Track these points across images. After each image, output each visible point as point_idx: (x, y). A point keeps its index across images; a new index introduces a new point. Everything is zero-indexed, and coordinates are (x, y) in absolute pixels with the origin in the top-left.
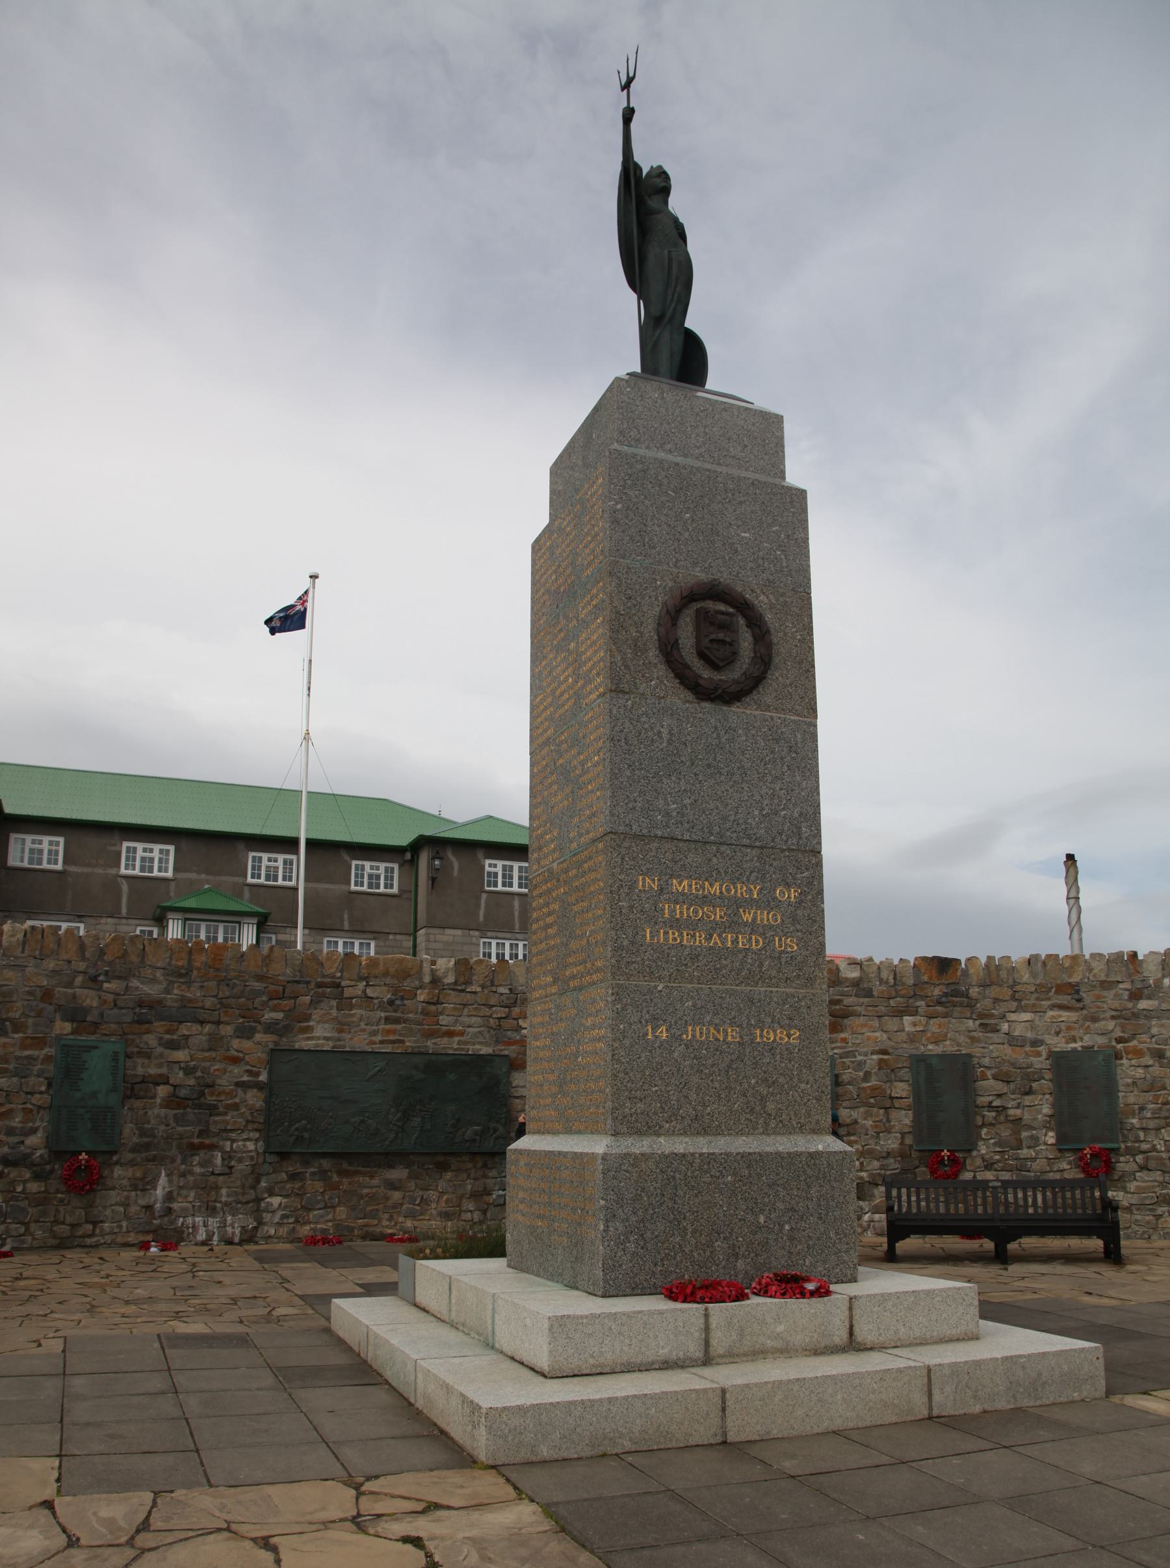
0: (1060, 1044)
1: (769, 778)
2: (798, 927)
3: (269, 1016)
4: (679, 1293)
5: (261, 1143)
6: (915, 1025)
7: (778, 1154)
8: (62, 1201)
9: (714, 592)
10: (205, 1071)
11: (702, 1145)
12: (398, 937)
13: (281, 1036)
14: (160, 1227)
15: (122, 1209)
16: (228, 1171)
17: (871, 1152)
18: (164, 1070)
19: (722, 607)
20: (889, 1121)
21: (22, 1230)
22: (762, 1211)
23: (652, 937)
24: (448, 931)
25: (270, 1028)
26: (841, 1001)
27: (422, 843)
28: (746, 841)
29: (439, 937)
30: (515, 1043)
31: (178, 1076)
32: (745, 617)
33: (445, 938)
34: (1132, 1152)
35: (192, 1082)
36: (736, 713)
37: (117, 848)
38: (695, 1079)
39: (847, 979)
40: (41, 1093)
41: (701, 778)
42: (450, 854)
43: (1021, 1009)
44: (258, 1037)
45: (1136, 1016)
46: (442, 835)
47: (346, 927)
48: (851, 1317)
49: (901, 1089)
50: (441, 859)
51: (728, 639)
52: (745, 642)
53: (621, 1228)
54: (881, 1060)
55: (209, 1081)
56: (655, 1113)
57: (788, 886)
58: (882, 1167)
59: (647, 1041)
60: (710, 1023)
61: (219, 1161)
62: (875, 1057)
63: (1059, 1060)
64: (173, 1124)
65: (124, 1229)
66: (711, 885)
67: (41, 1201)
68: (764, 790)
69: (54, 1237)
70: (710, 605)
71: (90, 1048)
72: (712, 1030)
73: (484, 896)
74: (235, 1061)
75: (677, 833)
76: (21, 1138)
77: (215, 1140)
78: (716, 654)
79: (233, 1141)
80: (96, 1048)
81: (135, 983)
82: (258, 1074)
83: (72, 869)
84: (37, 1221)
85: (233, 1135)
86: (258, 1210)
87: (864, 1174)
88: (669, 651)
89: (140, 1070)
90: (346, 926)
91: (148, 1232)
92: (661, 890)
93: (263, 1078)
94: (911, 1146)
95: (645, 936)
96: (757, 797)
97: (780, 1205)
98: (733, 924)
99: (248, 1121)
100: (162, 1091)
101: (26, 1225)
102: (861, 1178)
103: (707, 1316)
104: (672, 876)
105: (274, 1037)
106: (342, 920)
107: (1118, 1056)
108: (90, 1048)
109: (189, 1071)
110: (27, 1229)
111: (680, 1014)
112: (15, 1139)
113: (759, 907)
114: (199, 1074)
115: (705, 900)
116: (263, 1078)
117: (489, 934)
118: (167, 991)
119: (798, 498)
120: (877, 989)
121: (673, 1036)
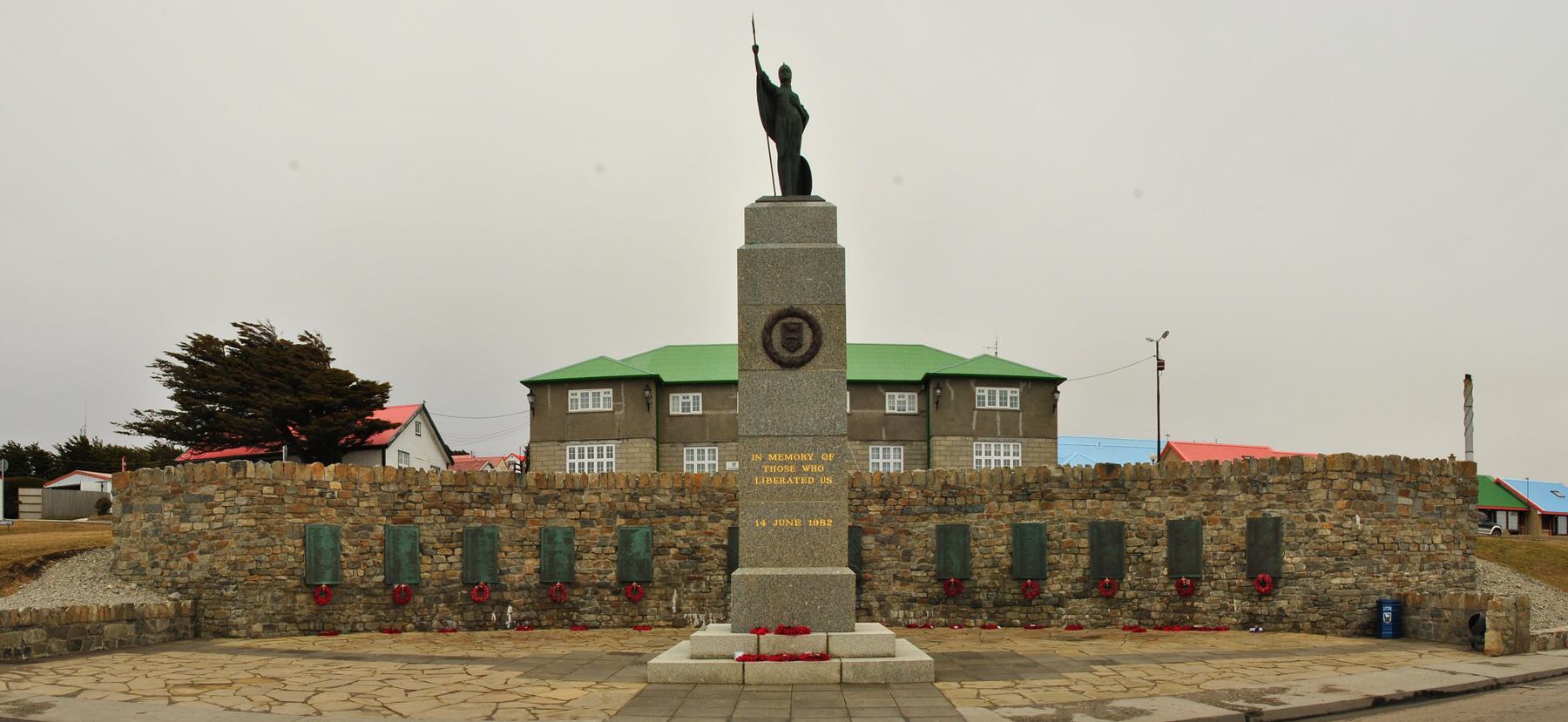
0: (1173, 516)
3: (727, 510)
4: (752, 632)
9: (791, 313)
11: (780, 571)
19: (796, 320)
27: (929, 378)
31: (681, 544)
34: (1209, 579)
36: (801, 373)
43: (1153, 495)
45: (1215, 499)
49: (1084, 542)
63: (1172, 525)
67: (616, 605)
70: (806, 325)
74: (710, 534)
78: (792, 343)
88: (767, 345)
98: (799, 472)
107: (1203, 523)
109: (685, 541)
115: (785, 463)
119: (840, 254)
120: (1073, 483)
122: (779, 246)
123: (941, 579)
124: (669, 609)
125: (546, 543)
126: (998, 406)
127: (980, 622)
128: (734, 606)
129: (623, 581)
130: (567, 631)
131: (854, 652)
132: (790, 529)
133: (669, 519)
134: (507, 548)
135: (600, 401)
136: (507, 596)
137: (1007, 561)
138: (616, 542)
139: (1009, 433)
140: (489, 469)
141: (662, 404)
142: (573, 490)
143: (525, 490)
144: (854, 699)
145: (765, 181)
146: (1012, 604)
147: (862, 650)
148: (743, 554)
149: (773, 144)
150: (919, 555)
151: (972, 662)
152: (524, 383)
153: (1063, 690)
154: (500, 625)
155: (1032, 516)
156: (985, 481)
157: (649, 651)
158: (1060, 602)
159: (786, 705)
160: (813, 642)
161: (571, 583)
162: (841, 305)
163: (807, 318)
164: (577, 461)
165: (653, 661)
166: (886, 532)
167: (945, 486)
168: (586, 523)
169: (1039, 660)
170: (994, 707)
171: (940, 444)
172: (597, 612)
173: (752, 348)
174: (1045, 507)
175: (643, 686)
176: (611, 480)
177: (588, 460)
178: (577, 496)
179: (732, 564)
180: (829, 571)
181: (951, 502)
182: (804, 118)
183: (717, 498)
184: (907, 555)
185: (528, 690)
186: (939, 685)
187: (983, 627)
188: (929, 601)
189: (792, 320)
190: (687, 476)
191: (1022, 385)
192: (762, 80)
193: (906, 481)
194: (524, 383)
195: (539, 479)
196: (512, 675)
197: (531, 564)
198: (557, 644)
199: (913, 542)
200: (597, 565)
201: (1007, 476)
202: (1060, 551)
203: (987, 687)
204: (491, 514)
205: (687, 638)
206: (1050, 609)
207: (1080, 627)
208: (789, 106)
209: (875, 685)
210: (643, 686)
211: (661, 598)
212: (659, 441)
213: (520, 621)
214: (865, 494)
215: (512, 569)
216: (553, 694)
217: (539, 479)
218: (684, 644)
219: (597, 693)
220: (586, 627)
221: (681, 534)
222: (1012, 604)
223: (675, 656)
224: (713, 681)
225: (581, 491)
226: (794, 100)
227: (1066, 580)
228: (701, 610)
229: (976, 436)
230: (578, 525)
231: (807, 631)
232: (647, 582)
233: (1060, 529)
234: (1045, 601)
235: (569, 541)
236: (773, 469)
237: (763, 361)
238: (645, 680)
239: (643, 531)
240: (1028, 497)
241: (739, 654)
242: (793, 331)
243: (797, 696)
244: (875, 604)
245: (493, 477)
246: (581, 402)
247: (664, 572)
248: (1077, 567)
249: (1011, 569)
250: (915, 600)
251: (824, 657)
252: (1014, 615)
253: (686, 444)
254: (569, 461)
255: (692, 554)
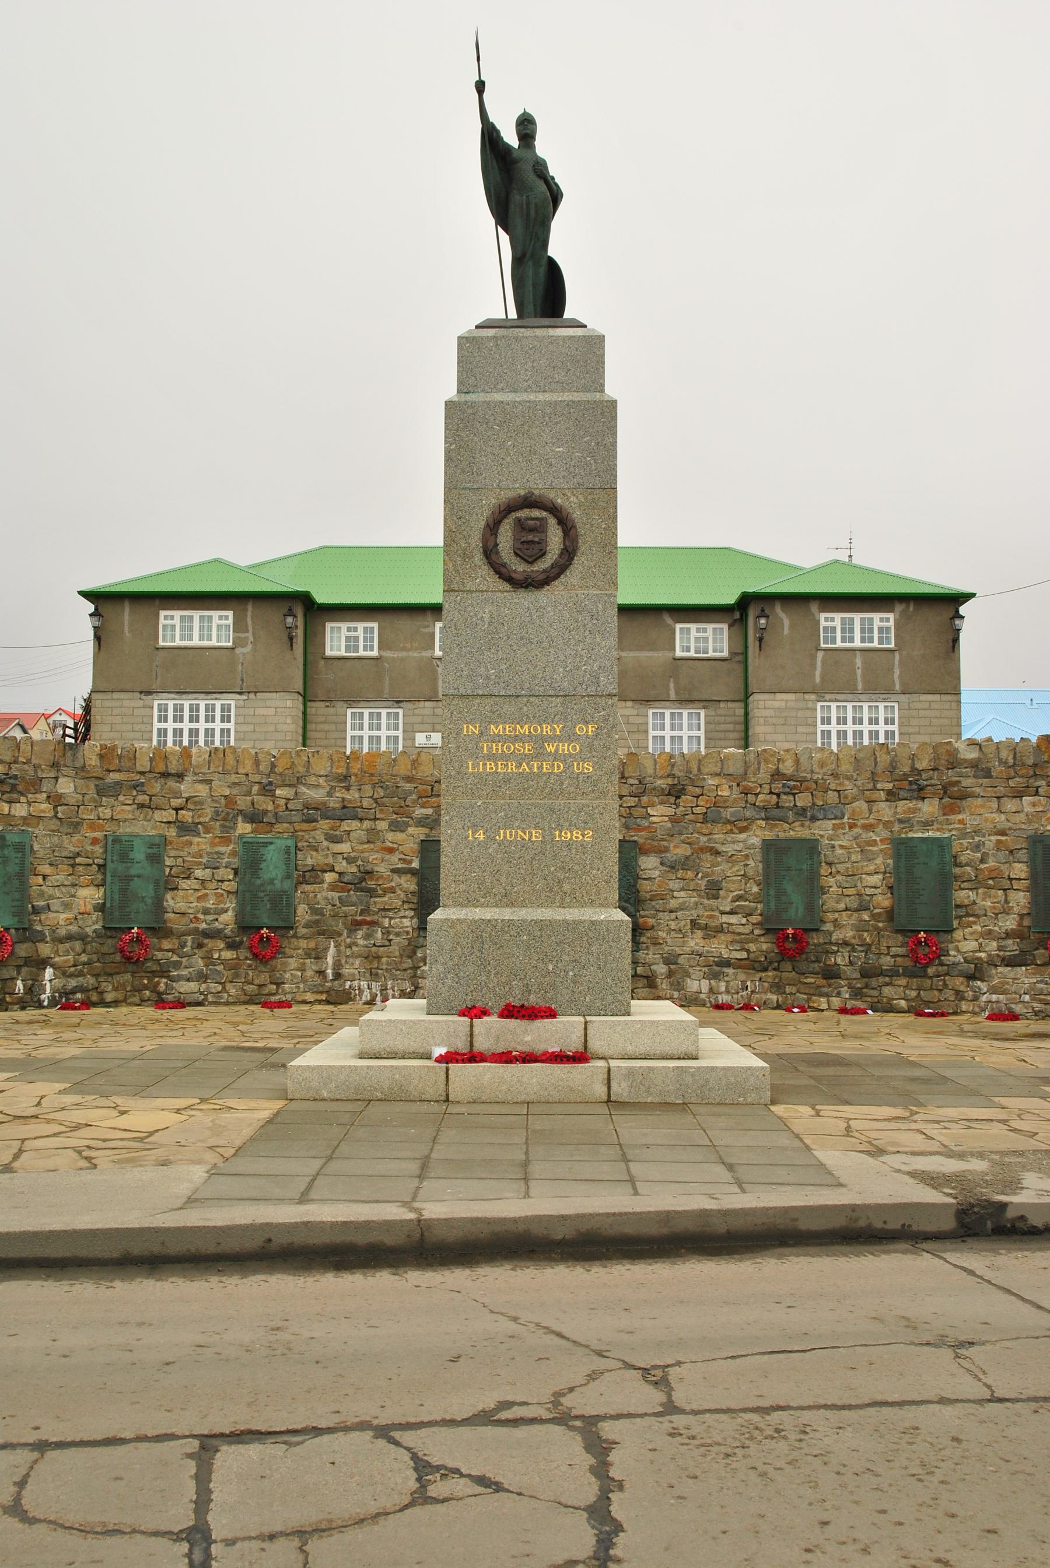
1: (573, 642)
2: (594, 753)
3: (419, 812)
4: (462, 1014)
5: (415, 920)
6: (1034, 805)
7: (565, 921)
8: (250, 966)
9: (529, 502)
10: (366, 861)
11: (507, 914)
12: (730, 705)
13: (431, 829)
14: (331, 989)
15: (299, 974)
16: (387, 943)
17: (990, 932)
18: (330, 860)
19: (536, 513)
20: (1007, 902)
21: (220, 988)
22: (551, 961)
23: (473, 768)
24: (779, 696)
25: (421, 822)
26: (960, 782)
27: (746, 601)
28: (551, 692)
29: (769, 703)
30: (644, 829)
31: (342, 865)
32: (555, 516)
33: (777, 704)
35: (354, 869)
36: (543, 596)
37: (430, 630)
38: (505, 867)
39: (965, 760)
40: (230, 880)
41: (515, 648)
42: (778, 609)
44: (411, 830)
46: (768, 590)
47: (673, 696)
48: (586, 1035)
49: (1020, 870)
50: (767, 617)
51: (536, 539)
52: (555, 539)
53: (441, 969)
54: (999, 842)
55: (369, 868)
56: (474, 892)
57: (587, 723)
58: (1000, 948)
59: (469, 841)
60: (519, 828)
61: (379, 935)
62: (992, 838)
64: (339, 905)
65: (302, 990)
66: (522, 727)
67: (233, 967)
68: (569, 651)
69: (246, 995)
70: (552, 521)
71: (266, 844)
72: (520, 832)
73: (820, 654)
74: (391, 851)
75: (496, 692)
76: (216, 917)
77: (375, 918)
78: (530, 546)
79: (391, 918)
80: (272, 843)
81: (303, 789)
82: (410, 862)
83: (387, 654)
84: (231, 982)
85: (391, 914)
86: (415, 976)
87: (983, 955)
88: (490, 553)
89: (309, 861)
90: (673, 696)
91: (322, 993)
92: (482, 733)
93: (415, 864)
94: (1029, 927)
95: (468, 767)
96: (562, 658)
97: (566, 958)
98: (539, 754)
99: (404, 902)
100: (329, 877)
101: (223, 984)
102: (980, 959)
103: (472, 1026)
104: (490, 723)
105: (427, 831)
106: (668, 688)
108: (266, 844)
109: (350, 861)
110: (224, 988)
111: (494, 822)
112: (210, 918)
113: (562, 741)
114: (359, 862)
115: (516, 739)
116: (415, 864)
117: (828, 697)
118: (330, 794)
119: (612, 405)
120: (997, 769)
121: (489, 837)
122: (510, 397)
123: (772, 929)
124: (321, 973)
125: (114, 862)
126: (857, 643)
127: (836, 1002)
128: (432, 972)
129: (246, 927)
130: (149, 1011)
131: (630, 1049)
132: (524, 845)
133: (324, 824)
134: (46, 869)
135: (214, 629)
136: (45, 950)
137: (884, 901)
138: (236, 862)
139: (877, 687)
140: (18, 734)
141: (313, 638)
142: (166, 775)
143: (82, 772)
144: (632, 1129)
145: (493, 297)
146: (893, 973)
147: (644, 1045)
148: (447, 886)
149: (505, 238)
150: (733, 888)
151: (831, 1071)
152: (87, 595)
153: (997, 1129)
154: (31, 1000)
155: (927, 824)
156: (845, 767)
157: (287, 1044)
158: (976, 972)
159: (519, 1138)
160: (560, 1032)
161: (160, 930)
162: (611, 490)
163: (555, 510)
164: (170, 726)
165: (297, 1062)
166: (679, 851)
167: (777, 775)
168: (185, 829)
169: (948, 1073)
170: (878, 1152)
171: (763, 705)
172: (202, 977)
173: (466, 556)
174: (949, 810)
175: (279, 1104)
176: (230, 759)
177: (182, 723)
178: (172, 783)
179: (426, 901)
180: (588, 914)
181: (787, 801)
182: (555, 197)
183: (406, 792)
184: (714, 889)
185: (78, 1116)
186: (778, 1109)
187: (843, 1011)
188: (751, 965)
189: (530, 532)
190: (355, 755)
191: (899, 607)
192: (490, 136)
193: (710, 767)
194: (87, 595)
195: (106, 754)
196: (48, 1088)
197: (89, 896)
198: (132, 1032)
199: (722, 868)
200: (201, 900)
201: (883, 759)
202: (976, 883)
203: (864, 1116)
204: (20, 810)
205: (355, 1023)
206: (959, 983)
207: (1015, 1017)
208: (531, 177)
209: (666, 1106)
210: (279, 1104)
211: (308, 955)
212: (306, 697)
213: (67, 993)
214: (642, 789)
215: (55, 904)
216: (123, 1122)
217: (106, 754)
218: (348, 1033)
219: (202, 1118)
220: (180, 1004)
221: (344, 849)
222: (893, 973)
223: (332, 1052)
224: (396, 1096)
225: (180, 776)
226: (540, 169)
227: (989, 934)
228: (374, 976)
229: (820, 693)
230: (172, 832)
231: (552, 1014)
232: (287, 928)
233: (977, 847)
234: (951, 970)
235: (156, 859)
236: (497, 748)
237: (483, 576)
238: (283, 1094)
239: (281, 843)
240: (920, 793)
241: (439, 1051)
242: (532, 530)
243: (536, 1124)
244: (661, 969)
245: (25, 748)
246: (176, 629)
247: (315, 911)
248: (1006, 911)
249: (890, 915)
250: (727, 963)
251: (580, 1057)
252: (896, 992)
253: (351, 702)
254: (157, 725)
255: (362, 882)
